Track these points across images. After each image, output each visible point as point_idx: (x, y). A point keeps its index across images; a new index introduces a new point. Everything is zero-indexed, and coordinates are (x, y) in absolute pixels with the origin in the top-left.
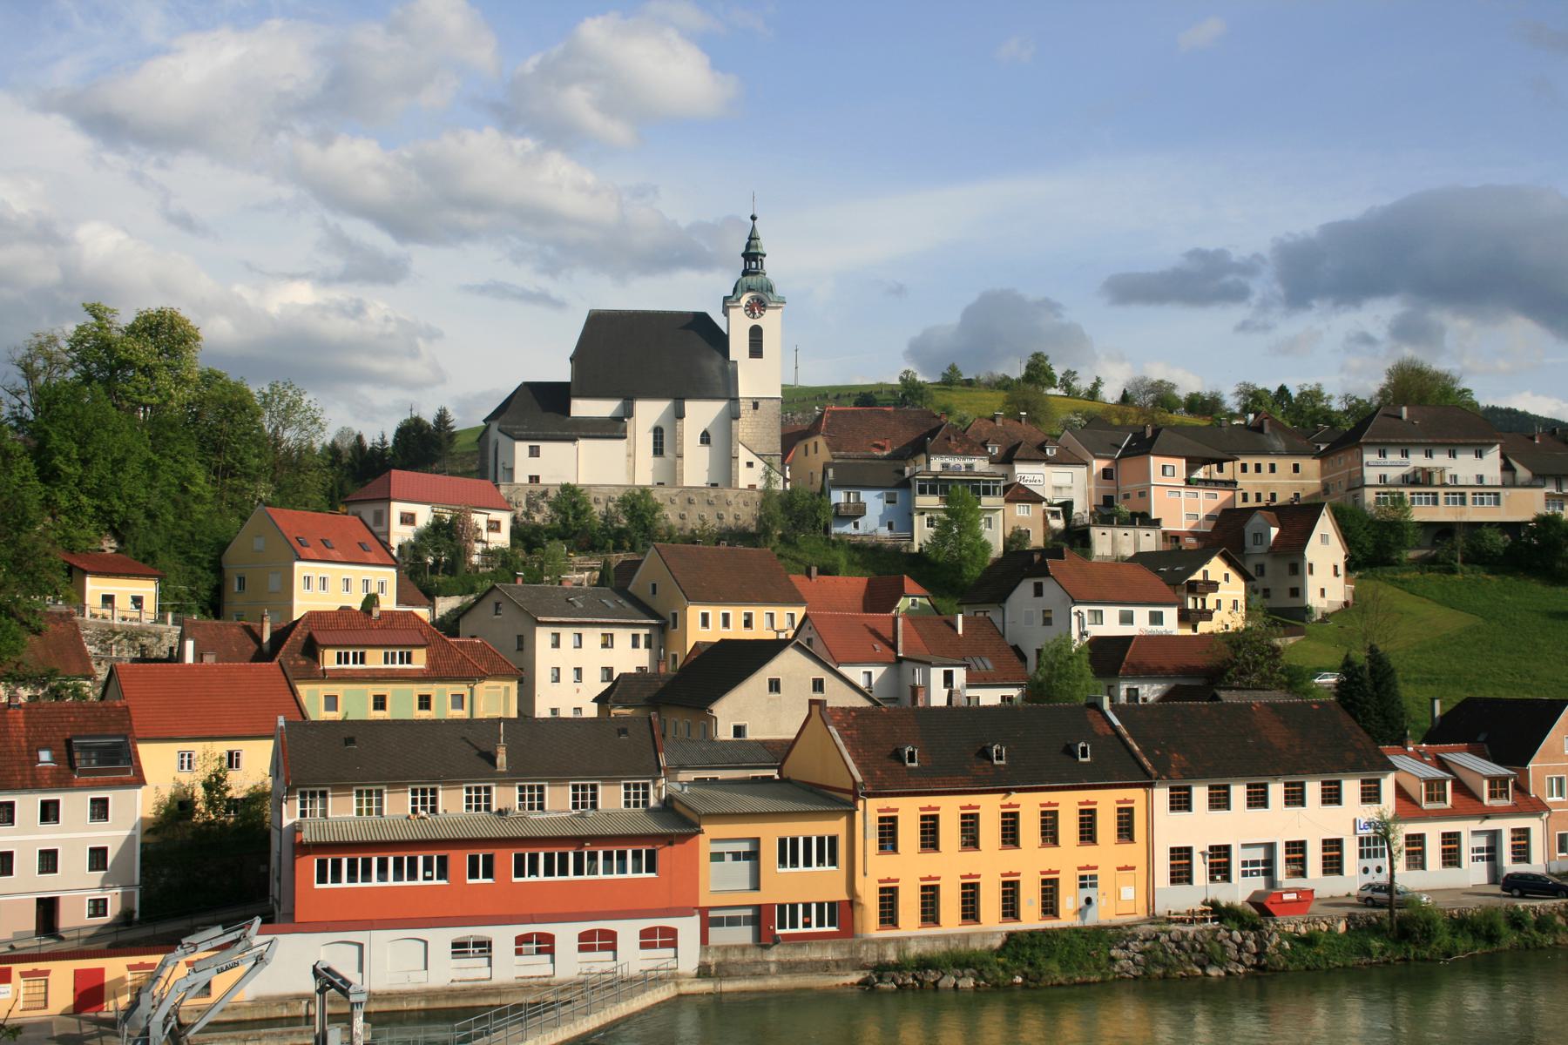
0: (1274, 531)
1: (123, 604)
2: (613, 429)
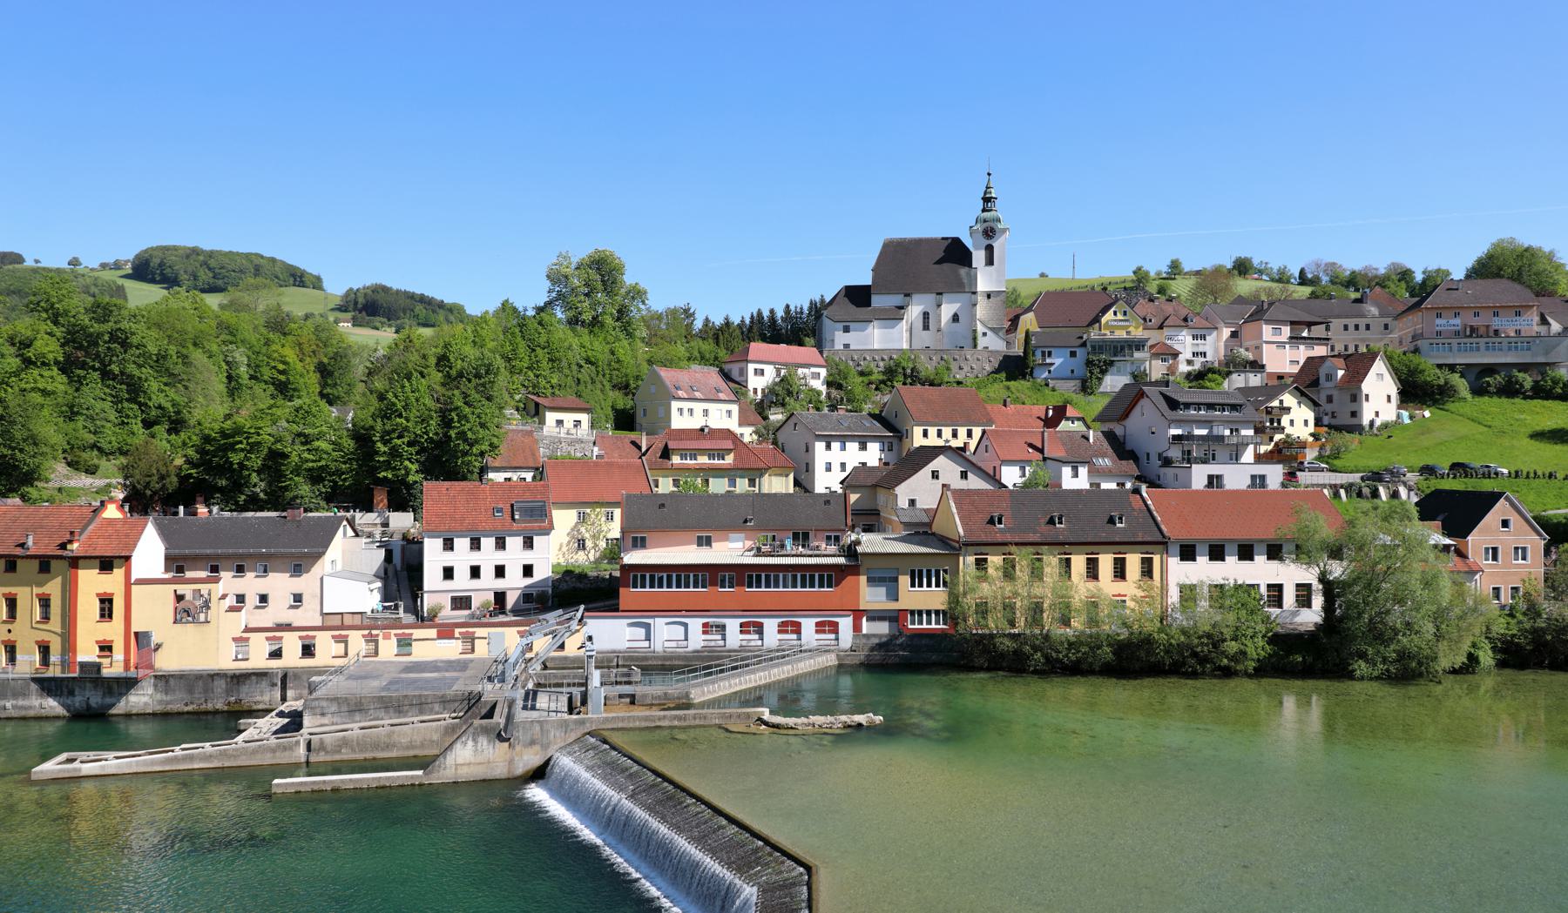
0: (1341, 373)
1: (569, 424)
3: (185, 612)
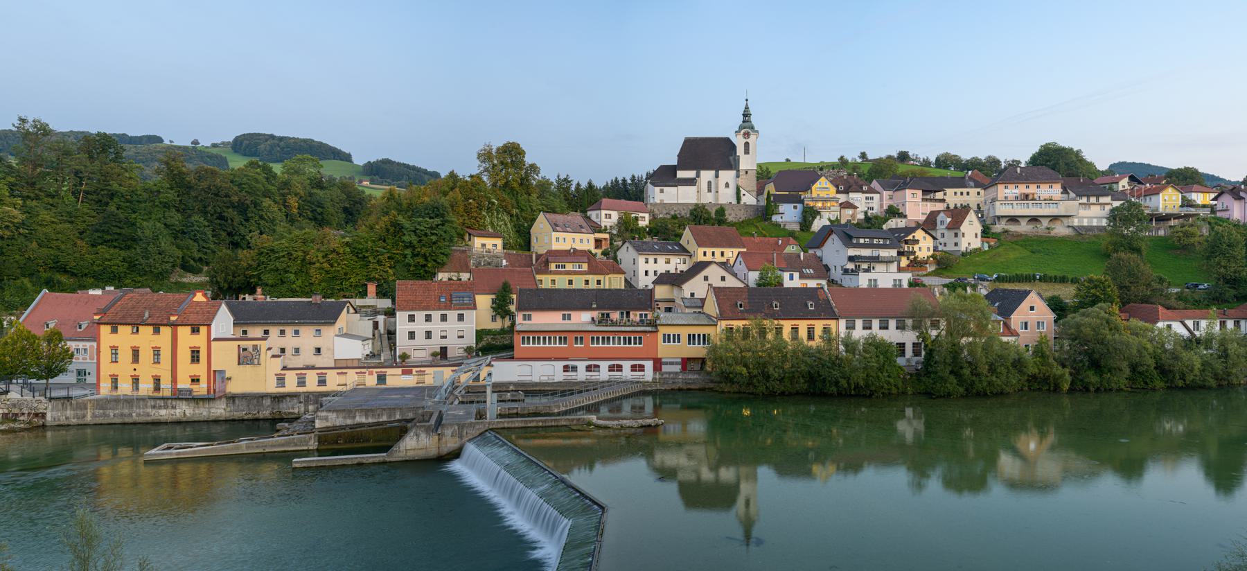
2: (691, 182)
3: (246, 358)
